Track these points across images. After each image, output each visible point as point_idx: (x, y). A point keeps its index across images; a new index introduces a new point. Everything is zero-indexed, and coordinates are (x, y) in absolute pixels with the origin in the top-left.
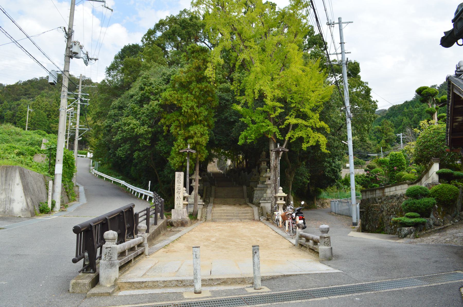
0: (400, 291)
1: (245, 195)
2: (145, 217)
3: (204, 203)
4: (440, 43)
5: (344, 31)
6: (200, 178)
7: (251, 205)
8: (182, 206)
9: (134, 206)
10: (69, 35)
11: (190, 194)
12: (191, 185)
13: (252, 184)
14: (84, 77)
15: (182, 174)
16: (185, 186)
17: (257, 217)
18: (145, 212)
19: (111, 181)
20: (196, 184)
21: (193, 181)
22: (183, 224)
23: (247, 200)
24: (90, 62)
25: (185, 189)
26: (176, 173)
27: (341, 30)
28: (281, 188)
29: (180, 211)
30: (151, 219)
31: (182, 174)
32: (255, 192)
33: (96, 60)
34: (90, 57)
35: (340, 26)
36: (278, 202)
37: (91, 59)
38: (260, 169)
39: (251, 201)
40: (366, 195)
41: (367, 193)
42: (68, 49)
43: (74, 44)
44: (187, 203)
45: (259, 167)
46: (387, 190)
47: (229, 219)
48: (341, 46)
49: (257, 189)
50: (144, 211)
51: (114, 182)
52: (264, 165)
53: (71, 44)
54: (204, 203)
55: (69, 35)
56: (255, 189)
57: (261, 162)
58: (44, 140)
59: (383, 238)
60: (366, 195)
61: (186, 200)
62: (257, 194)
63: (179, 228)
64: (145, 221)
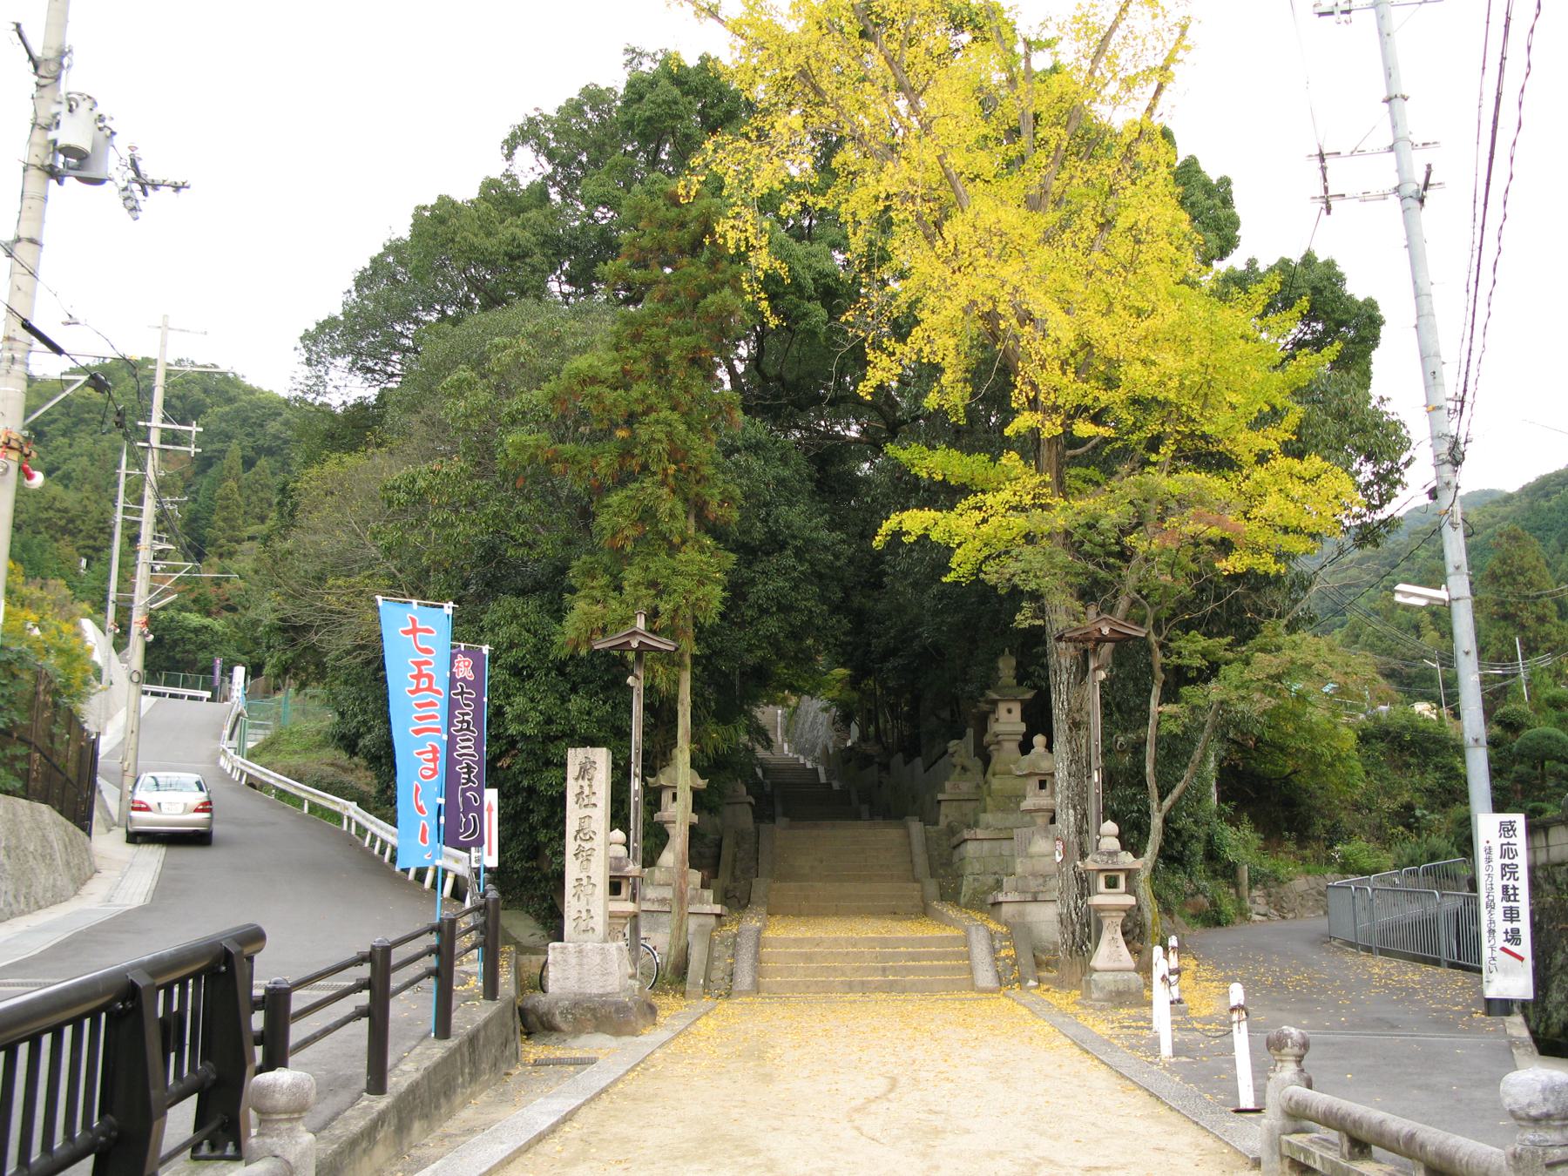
0: (55, 396)
3: (718, 909)
5: (1400, 41)
6: (702, 783)
7: (951, 912)
8: (599, 923)
9: (255, 937)
10: (48, 69)
11: (650, 860)
12: (657, 817)
15: (601, 757)
16: (619, 818)
19: (302, 800)
20: (679, 814)
21: (666, 797)
22: (607, 1017)
23: (932, 887)
24: (154, 203)
25: (619, 835)
26: (571, 752)
27: (1384, 35)
28: (1110, 827)
29: (587, 955)
30: (399, 1009)
31: (601, 757)
32: (970, 849)
33: (177, 188)
34: (150, 171)
35: (1381, 18)
36: (1096, 900)
37: (155, 186)
38: (987, 738)
39: (950, 895)
42: (39, 136)
43: (64, 108)
44: (629, 907)
45: (982, 728)
48: (1392, 112)
49: (980, 833)
51: (314, 808)
52: (1008, 720)
53: (55, 109)
54: (718, 909)
55: (48, 69)
56: (966, 834)
57: (995, 703)
61: (625, 891)
63: (584, 1039)
64: (365, 1021)
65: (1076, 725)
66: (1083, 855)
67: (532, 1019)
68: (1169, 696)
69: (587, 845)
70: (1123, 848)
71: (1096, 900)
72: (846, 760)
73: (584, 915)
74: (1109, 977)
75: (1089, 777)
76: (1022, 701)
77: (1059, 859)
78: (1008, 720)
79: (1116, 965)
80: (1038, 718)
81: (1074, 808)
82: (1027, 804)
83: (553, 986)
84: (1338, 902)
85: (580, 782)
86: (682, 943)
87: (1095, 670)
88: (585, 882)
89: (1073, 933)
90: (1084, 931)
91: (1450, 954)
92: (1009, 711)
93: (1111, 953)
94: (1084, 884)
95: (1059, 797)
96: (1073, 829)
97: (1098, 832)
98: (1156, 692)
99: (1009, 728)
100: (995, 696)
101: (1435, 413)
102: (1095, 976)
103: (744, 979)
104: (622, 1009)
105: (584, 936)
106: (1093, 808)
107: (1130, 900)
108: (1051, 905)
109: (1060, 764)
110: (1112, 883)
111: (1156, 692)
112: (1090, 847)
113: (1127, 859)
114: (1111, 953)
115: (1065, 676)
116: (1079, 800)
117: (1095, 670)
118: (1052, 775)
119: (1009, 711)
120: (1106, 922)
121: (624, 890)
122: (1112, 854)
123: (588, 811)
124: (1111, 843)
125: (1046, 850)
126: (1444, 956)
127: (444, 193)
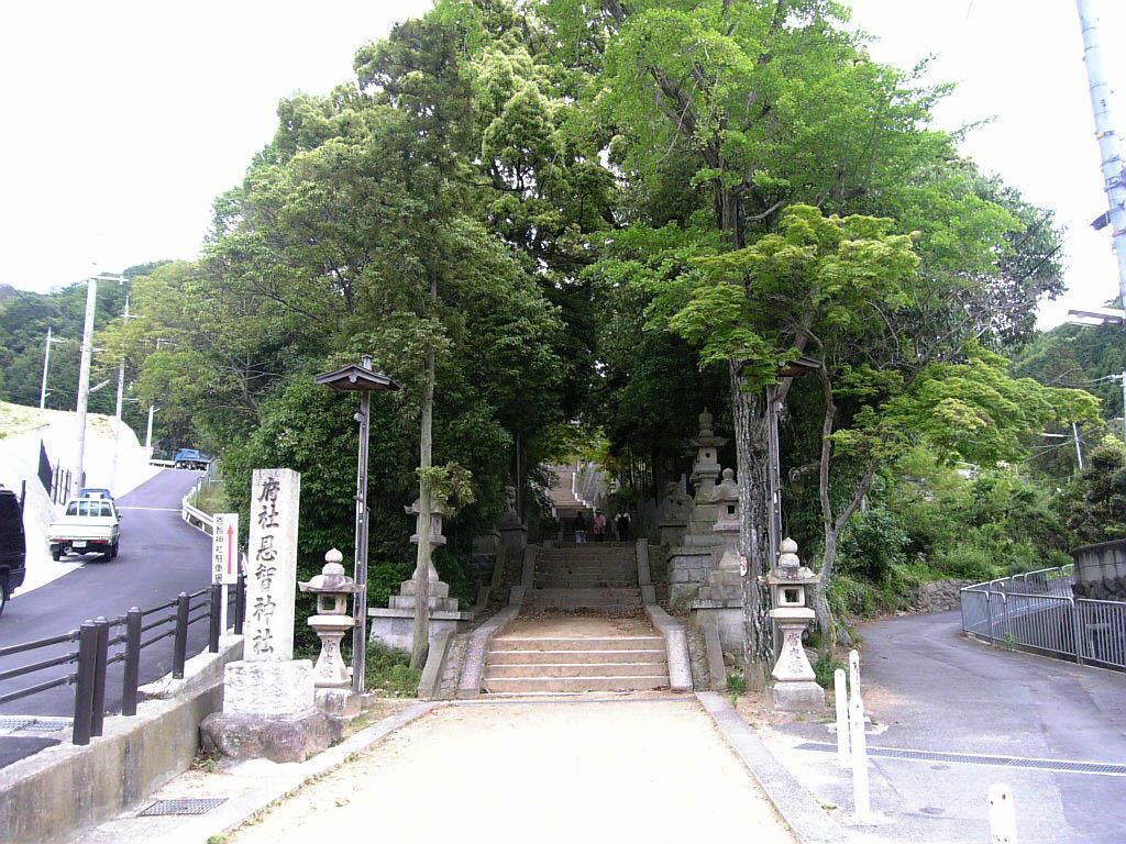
1: (644, 575)
2: (173, 625)
4: (71, 413)
7: (657, 614)
13: (667, 536)
14: (184, 263)
17: (680, 677)
18: (174, 611)
22: (273, 742)
23: (649, 592)
32: (677, 564)
36: (777, 613)
40: (1102, 566)
41: (1108, 557)
46: (289, 484)
47: (579, 688)
50: (172, 605)
52: (707, 463)
56: (677, 551)
57: (696, 449)
58: (604, 163)
59: (629, 631)
60: (1102, 566)
62: (683, 571)
65: (758, 454)
66: (765, 569)
67: (207, 739)
68: (844, 421)
69: (268, 565)
70: (802, 565)
71: (777, 613)
72: (615, 502)
73: (264, 634)
74: (791, 687)
75: (769, 499)
76: (717, 448)
77: (743, 573)
78: (707, 463)
79: (799, 676)
80: (728, 458)
81: (757, 528)
82: (717, 527)
83: (228, 708)
84: (970, 603)
85: (264, 502)
86: (424, 645)
87: (772, 402)
88: (265, 601)
89: (757, 640)
90: (768, 639)
91: (1086, 651)
92: (708, 455)
93: (793, 663)
94: (767, 601)
95: (741, 520)
96: (755, 546)
97: (778, 549)
98: (828, 422)
99: (707, 469)
100: (697, 444)
101: (1106, 140)
102: (778, 686)
103: (470, 681)
104: (288, 732)
105: (263, 656)
106: (773, 526)
107: (809, 613)
108: (740, 612)
109: (741, 491)
110: (792, 596)
111: (828, 422)
112: (772, 560)
113: (806, 574)
114: (793, 663)
115: (747, 411)
116: (760, 518)
117: (772, 402)
118: (737, 501)
119: (708, 455)
120: (787, 635)
121: (338, 606)
122: (792, 570)
123: (272, 531)
124: (791, 559)
125: (735, 563)
126: (1080, 654)
127: (288, 93)
